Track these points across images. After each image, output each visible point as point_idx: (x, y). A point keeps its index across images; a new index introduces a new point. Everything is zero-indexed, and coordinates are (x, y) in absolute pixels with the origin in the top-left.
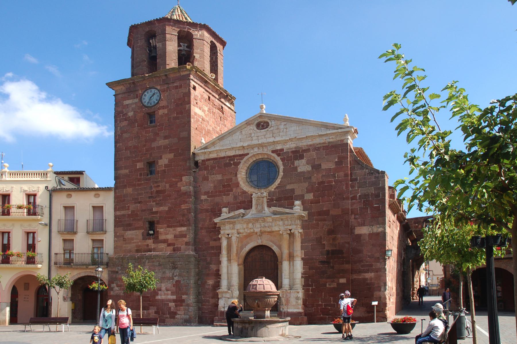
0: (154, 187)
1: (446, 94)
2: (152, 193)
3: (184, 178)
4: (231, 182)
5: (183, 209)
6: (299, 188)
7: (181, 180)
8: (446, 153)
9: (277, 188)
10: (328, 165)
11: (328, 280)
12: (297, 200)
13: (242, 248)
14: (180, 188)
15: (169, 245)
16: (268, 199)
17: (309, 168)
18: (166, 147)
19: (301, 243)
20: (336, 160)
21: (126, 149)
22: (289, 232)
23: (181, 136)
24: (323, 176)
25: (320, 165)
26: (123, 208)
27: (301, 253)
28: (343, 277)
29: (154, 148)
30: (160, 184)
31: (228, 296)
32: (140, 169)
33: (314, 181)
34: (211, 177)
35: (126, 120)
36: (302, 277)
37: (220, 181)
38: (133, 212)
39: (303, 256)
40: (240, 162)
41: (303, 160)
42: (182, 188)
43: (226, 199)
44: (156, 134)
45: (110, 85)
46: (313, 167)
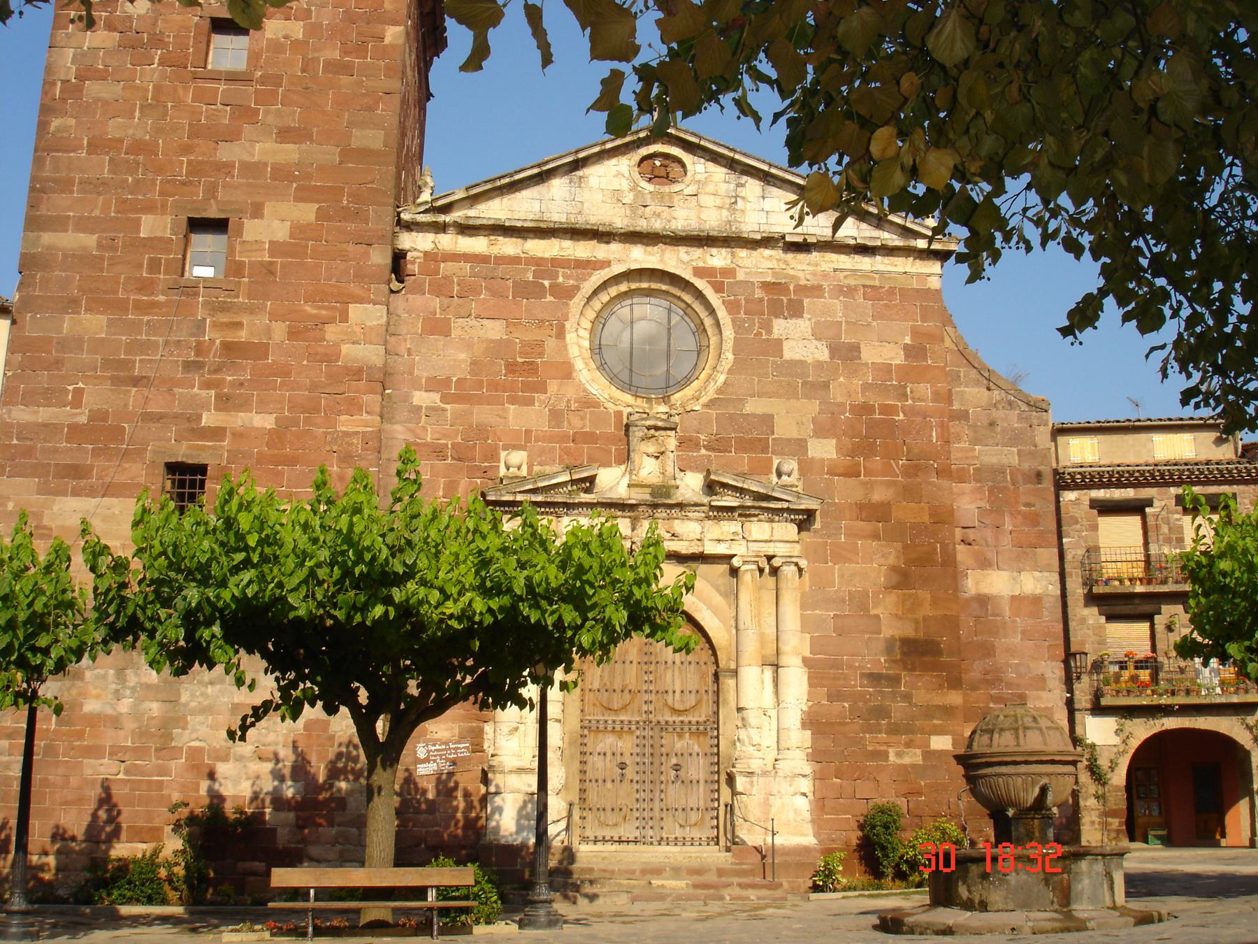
0: (215, 325)
3: (355, 311)
4: (541, 355)
5: (346, 434)
6: (791, 416)
7: (345, 318)
8: (359, 559)
9: (711, 404)
10: (883, 351)
11: (894, 738)
14: (337, 345)
17: (821, 353)
18: (282, 174)
19: (803, 607)
20: (908, 340)
21: (93, 147)
24: (866, 387)
25: (855, 348)
26: (51, 396)
28: (940, 731)
29: (229, 166)
32: (152, 243)
33: (840, 399)
34: (459, 327)
37: (497, 348)
38: (98, 417)
39: (807, 654)
40: (578, 288)
41: (799, 321)
42: (345, 348)
43: (515, 417)
44: (245, 114)
45: (1095, 328)
46: (835, 350)
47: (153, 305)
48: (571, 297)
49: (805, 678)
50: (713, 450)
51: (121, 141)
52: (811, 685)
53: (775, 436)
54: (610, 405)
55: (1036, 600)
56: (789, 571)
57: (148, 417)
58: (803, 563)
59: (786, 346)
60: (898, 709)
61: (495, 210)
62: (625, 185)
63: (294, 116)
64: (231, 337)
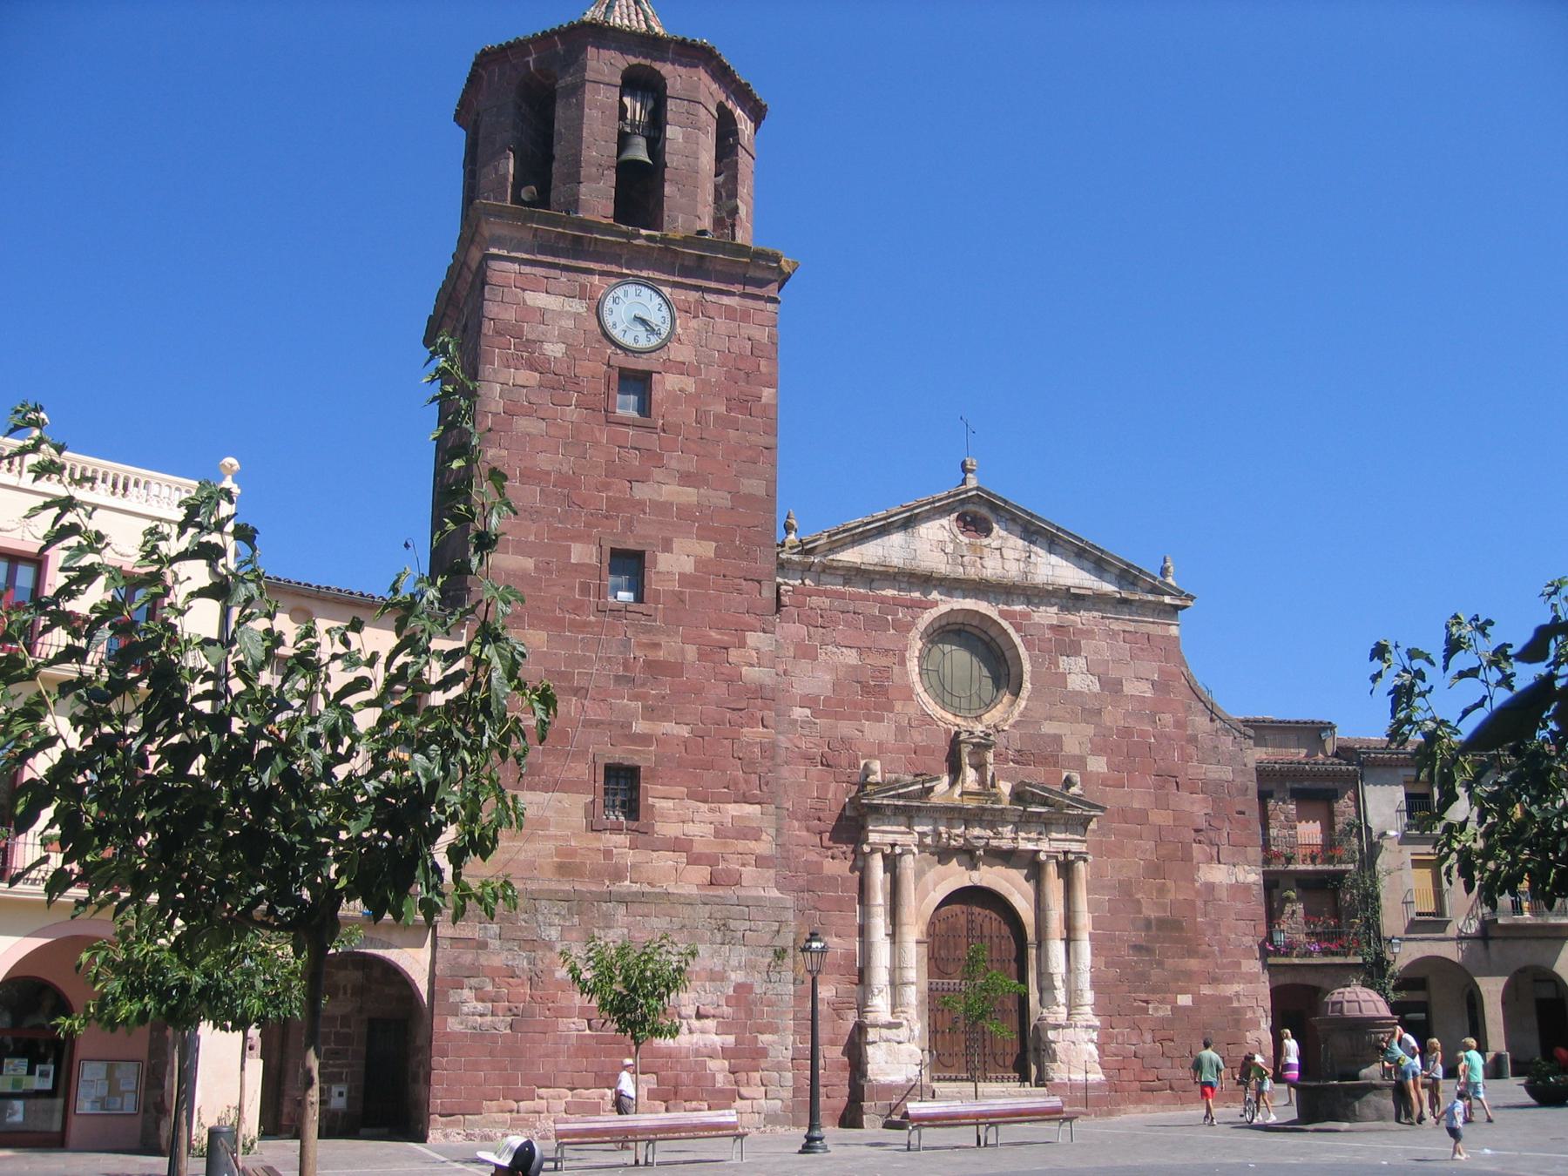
0: (639, 645)
2: (626, 666)
3: (753, 638)
6: (1074, 737)
11: (1151, 997)
15: (694, 860)
18: (685, 513)
23: (744, 490)
24: (1127, 714)
30: (663, 640)
32: (578, 568)
35: (532, 368)
44: (654, 458)
47: (586, 624)
48: (909, 631)
51: (548, 473)
55: (1246, 887)
57: (588, 724)
59: (1070, 679)
60: (1156, 974)
61: (850, 556)
62: (945, 536)
63: (691, 465)
64: (652, 655)
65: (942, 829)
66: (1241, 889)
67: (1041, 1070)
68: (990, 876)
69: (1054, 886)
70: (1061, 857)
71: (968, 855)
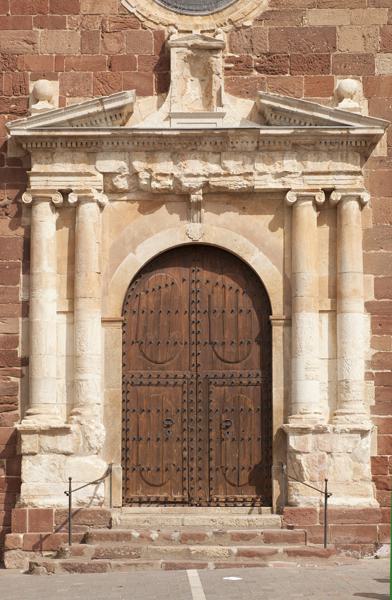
1: (354, 27)
12: (345, 74)
13: (118, 254)
16: (228, 60)
22: (59, 199)
27: (366, 282)
31: (64, 443)
36: (369, 376)
39: (371, 298)
43: (49, 42)
49: (369, 324)
50: (266, 71)
52: (374, 332)
53: (338, 52)
54: (148, 24)
56: (352, 206)
58: (366, 197)
65: (138, 165)
66: (386, 173)
67: (285, 490)
68: (216, 228)
69: (312, 231)
70: (321, 198)
71: (179, 199)
